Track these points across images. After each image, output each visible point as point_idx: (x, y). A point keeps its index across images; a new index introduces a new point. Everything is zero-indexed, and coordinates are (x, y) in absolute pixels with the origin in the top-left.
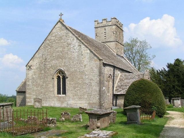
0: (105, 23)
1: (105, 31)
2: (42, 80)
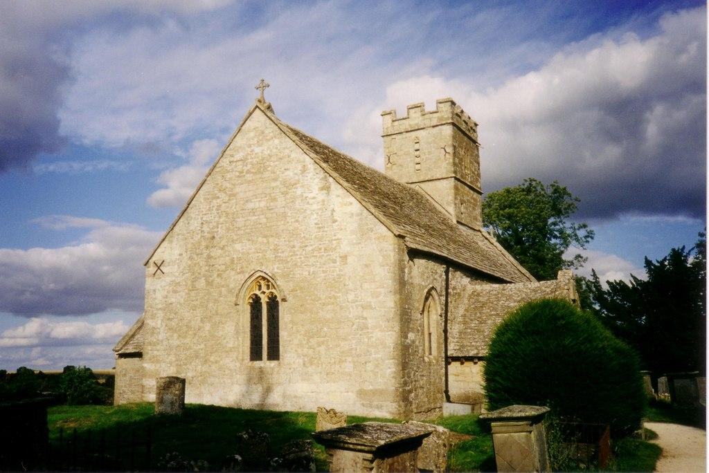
0: (416, 119)
1: (417, 146)
2: (199, 312)
